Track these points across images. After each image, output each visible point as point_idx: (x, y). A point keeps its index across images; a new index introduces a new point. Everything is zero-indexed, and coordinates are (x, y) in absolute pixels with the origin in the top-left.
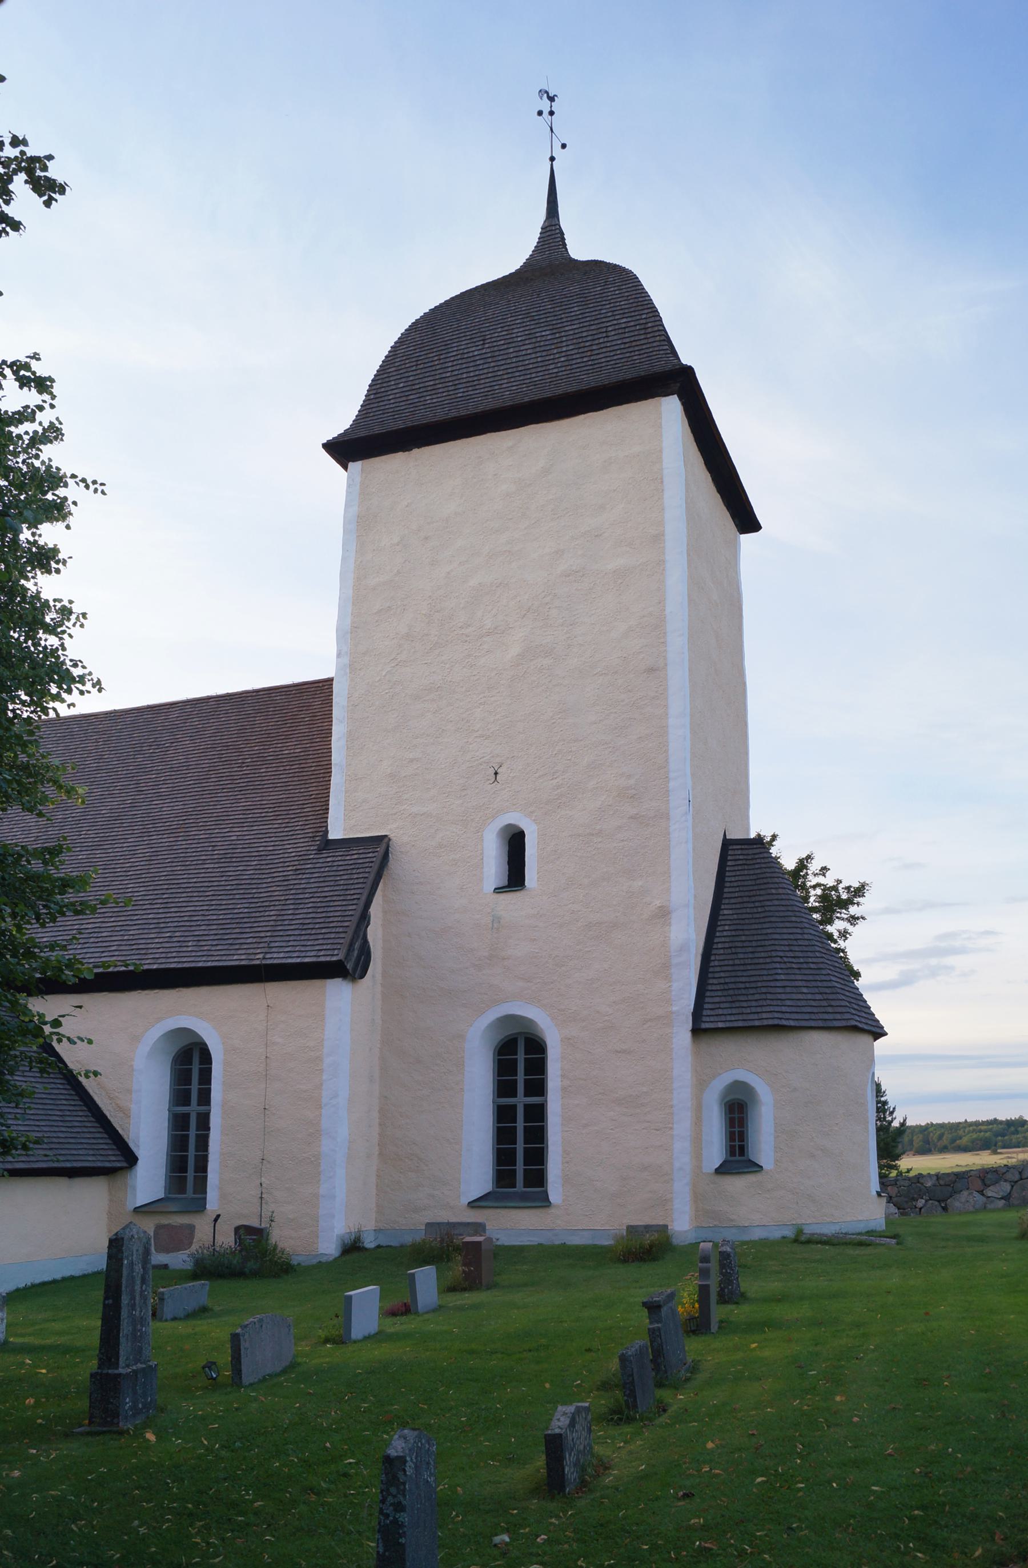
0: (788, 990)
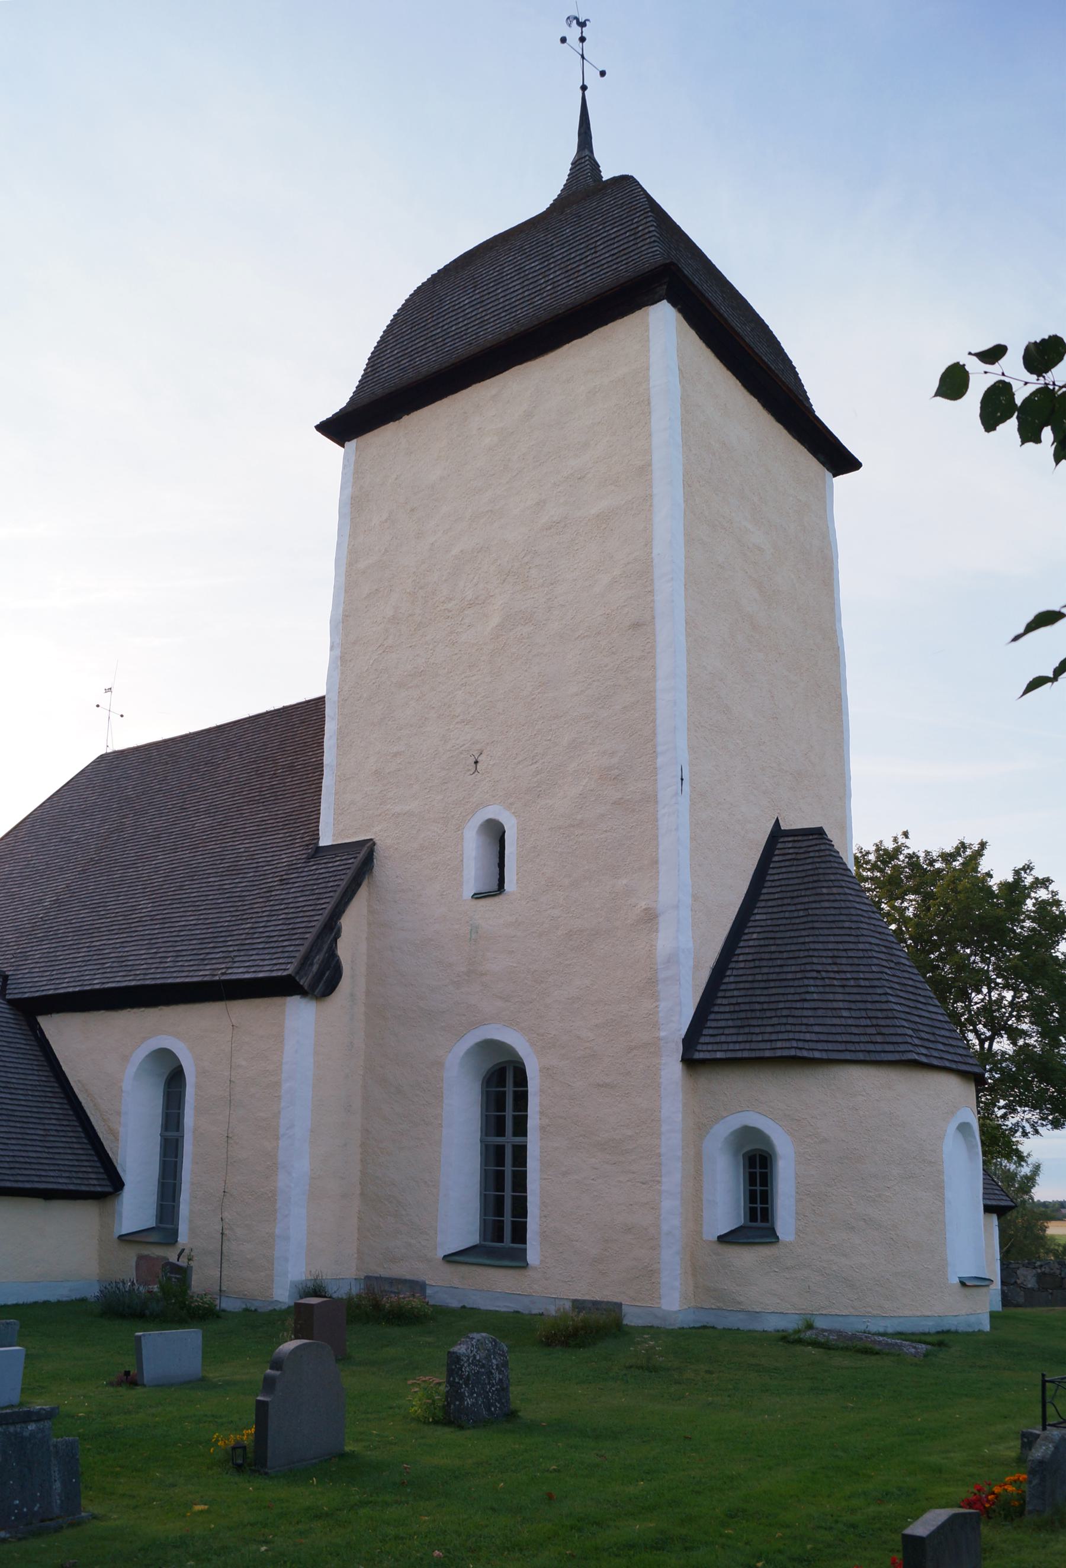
0: (820, 1013)
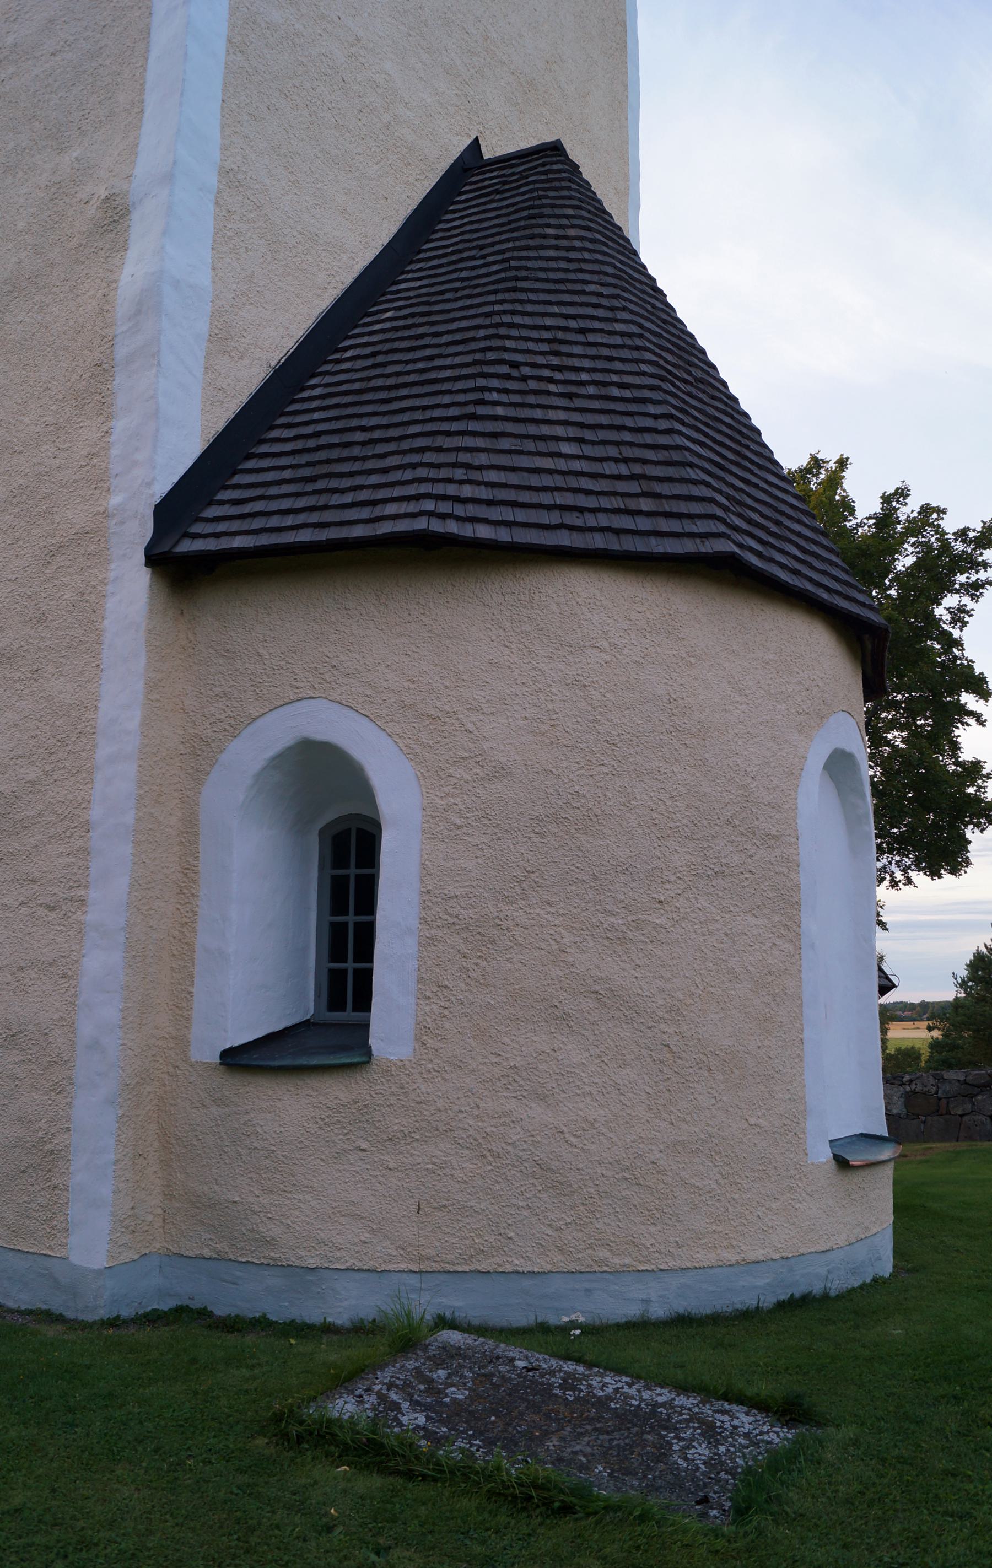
0: (505, 444)
